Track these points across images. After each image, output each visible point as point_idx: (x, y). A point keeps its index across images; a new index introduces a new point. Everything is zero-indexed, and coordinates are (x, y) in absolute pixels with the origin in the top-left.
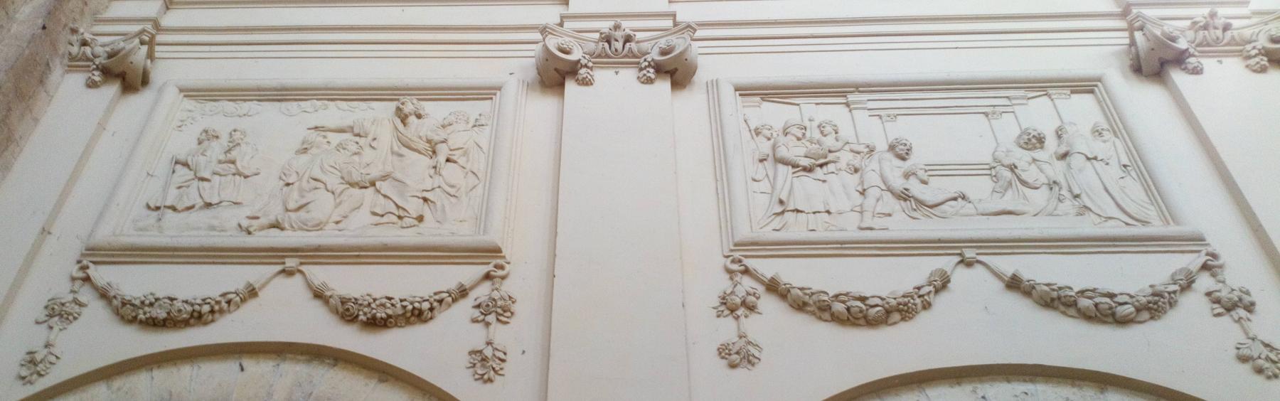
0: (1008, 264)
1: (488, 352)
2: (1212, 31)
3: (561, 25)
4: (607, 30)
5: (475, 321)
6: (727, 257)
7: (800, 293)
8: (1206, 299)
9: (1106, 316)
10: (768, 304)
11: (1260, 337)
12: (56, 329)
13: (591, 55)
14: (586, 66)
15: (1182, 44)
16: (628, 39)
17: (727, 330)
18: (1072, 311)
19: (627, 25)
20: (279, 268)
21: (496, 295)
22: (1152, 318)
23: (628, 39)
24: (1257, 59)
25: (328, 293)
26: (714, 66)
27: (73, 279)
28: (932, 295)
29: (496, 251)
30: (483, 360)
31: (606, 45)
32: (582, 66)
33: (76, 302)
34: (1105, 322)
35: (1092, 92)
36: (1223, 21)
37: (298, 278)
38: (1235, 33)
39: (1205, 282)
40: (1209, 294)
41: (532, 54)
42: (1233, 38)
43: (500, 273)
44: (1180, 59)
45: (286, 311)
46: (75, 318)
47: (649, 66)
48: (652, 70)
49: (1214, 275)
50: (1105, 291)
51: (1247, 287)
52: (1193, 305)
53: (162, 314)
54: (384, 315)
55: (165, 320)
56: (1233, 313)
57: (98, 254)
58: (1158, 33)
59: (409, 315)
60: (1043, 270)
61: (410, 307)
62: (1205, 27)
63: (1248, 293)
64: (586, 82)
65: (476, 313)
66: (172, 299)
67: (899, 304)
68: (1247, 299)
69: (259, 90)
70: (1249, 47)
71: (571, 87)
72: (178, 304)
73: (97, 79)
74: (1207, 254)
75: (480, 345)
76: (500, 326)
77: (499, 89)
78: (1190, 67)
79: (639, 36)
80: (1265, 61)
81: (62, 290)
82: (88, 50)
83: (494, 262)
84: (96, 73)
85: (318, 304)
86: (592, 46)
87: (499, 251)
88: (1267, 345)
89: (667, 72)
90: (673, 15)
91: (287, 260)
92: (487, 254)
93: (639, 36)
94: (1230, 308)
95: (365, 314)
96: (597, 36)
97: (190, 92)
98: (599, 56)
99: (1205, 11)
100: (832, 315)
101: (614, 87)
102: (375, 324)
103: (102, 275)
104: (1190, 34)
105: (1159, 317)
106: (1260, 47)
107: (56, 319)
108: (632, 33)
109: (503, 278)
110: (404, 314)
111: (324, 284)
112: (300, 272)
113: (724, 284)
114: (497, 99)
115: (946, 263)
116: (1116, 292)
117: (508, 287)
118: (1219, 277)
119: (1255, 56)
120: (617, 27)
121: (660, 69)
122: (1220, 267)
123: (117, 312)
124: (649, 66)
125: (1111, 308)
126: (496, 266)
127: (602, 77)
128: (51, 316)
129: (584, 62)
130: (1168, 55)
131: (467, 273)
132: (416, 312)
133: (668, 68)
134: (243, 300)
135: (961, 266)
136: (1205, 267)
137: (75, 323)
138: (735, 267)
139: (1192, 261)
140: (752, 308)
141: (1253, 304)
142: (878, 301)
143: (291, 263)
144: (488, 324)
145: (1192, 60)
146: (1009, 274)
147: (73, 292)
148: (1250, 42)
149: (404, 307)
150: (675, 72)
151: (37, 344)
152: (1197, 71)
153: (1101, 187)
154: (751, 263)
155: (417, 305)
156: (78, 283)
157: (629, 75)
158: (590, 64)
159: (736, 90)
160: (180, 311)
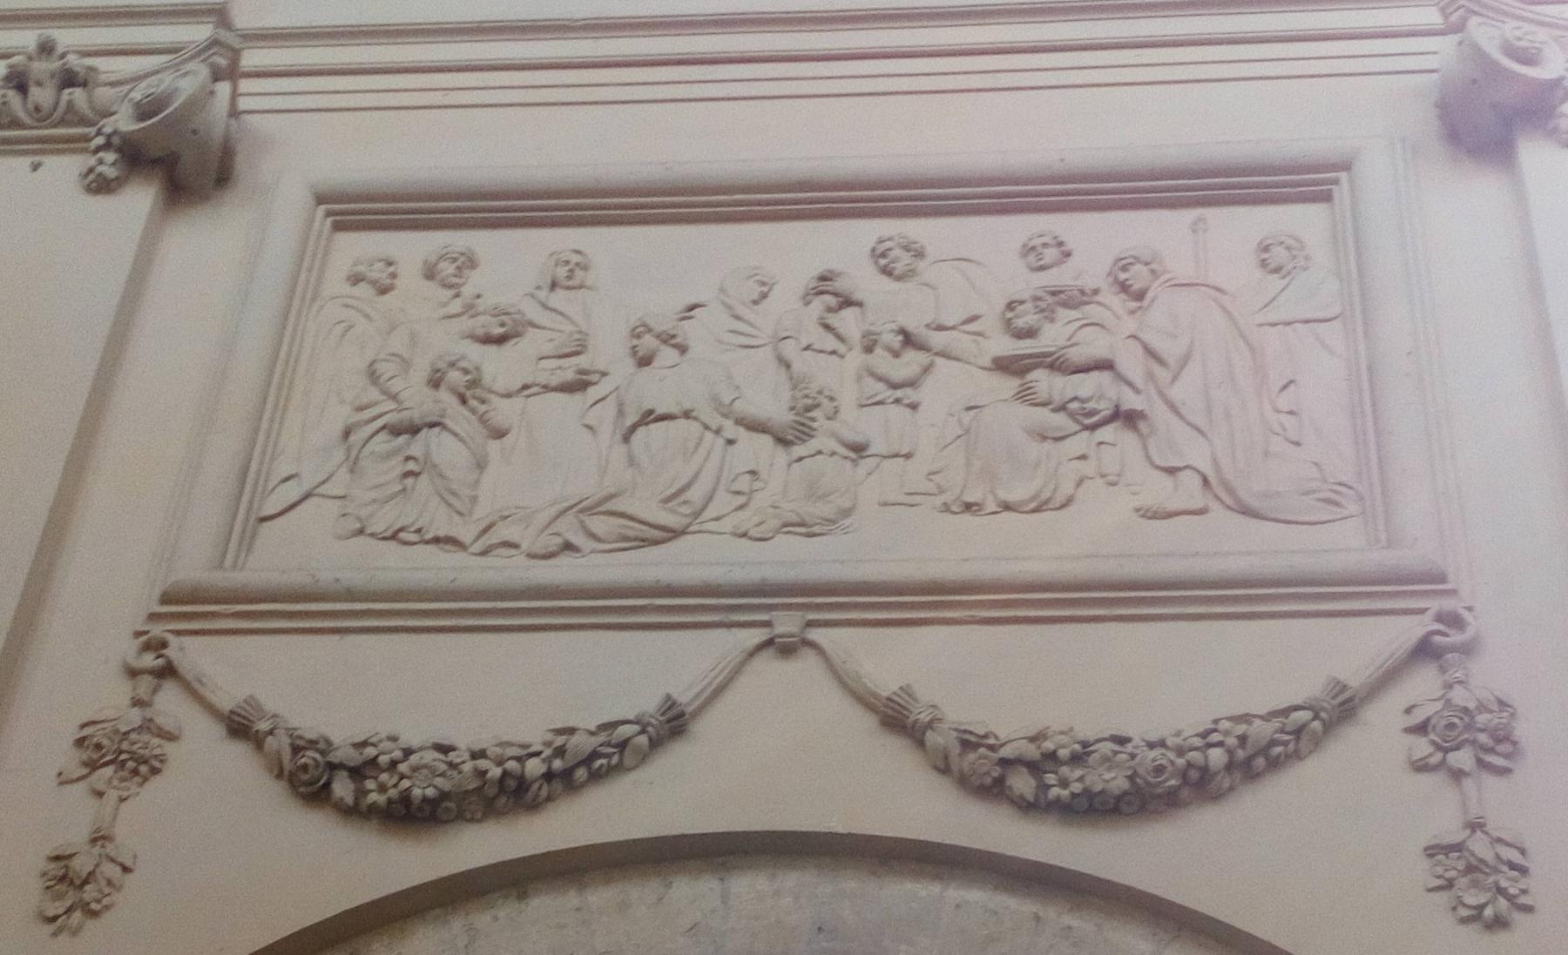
1: (1480, 847)
5: (1421, 767)
12: (113, 795)
16: (69, 79)
20: (756, 636)
21: (1459, 696)
26: (304, 143)
27: (133, 673)
29: (1433, 579)
30: (1470, 869)
33: (147, 726)
35: (1326, 197)
37: (807, 663)
45: (781, 747)
46: (155, 771)
47: (107, 146)
49: (1443, 670)
53: (1115, 781)
54: (430, 792)
55: (1119, 799)
59: (491, 791)
61: (496, 772)
73: (111, 172)
74: (1439, 618)
75: (1452, 831)
76: (1490, 780)
81: (111, 699)
82: (77, 95)
83: (1434, 605)
84: (110, 157)
87: (1442, 579)
89: (156, 162)
93: (110, 67)
95: (382, 789)
97: (354, 210)
102: (1095, 809)
107: (108, 771)
108: (73, 61)
110: (478, 790)
111: (251, 701)
112: (812, 645)
117: (1487, 677)
120: (46, 49)
124: (107, 146)
126: (1439, 618)
128: (93, 766)
131: (1356, 647)
132: (512, 784)
133: (155, 152)
134: (656, 744)
135: (768, 653)
137: (156, 783)
138: (149, 660)
143: (786, 624)
144: (1458, 775)
147: (137, 703)
149: (482, 774)
151: (75, 836)
155: (511, 765)
156: (146, 682)
159: (321, 199)
160: (1159, 770)
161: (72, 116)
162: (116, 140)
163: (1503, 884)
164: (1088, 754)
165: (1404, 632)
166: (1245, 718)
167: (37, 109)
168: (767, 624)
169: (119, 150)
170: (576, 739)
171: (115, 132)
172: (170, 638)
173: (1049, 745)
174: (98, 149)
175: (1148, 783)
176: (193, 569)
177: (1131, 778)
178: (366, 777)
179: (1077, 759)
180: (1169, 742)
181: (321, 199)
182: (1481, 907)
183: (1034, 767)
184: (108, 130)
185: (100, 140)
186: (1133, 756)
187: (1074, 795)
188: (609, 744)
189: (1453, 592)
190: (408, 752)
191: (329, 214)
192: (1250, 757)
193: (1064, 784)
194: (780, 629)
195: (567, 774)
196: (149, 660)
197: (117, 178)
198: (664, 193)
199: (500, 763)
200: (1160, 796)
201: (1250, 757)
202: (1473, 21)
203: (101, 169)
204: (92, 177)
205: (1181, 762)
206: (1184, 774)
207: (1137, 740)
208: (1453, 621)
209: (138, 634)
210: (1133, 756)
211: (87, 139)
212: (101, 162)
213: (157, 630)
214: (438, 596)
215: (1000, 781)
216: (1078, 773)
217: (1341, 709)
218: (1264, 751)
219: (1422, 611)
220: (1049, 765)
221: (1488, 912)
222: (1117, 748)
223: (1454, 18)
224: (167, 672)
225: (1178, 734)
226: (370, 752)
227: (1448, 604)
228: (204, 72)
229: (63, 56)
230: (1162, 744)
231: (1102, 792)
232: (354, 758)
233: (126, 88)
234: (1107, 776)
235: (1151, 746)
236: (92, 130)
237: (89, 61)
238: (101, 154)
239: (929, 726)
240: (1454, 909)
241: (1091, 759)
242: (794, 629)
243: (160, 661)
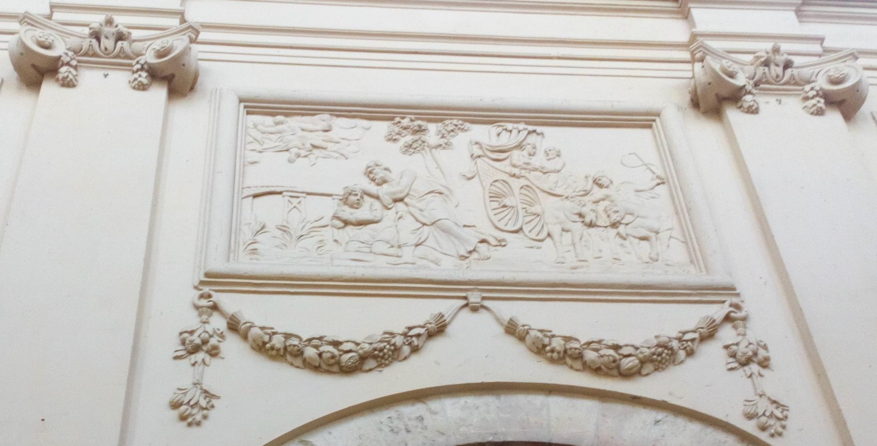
0: (508, 310)
2: (773, 67)
3: (50, 17)
4: (95, 25)
6: (196, 288)
7: (539, 335)
8: (724, 352)
9: (330, 365)
10: (232, 346)
11: (768, 394)
13: (76, 52)
14: (68, 64)
15: (740, 80)
16: (120, 37)
17: (183, 375)
18: (298, 362)
19: (121, 20)
20: (464, 302)
22: (656, 370)
23: (120, 37)
24: (814, 101)
26: (227, 75)
28: (696, 343)
29: (729, 289)
31: (94, 41)
32: (63, 65)
34: (613, 376)
35: (650, 127)
36: (786, 56)
37: (483, 315)
38: (795, 72)
39: (727, 334)
40: (726, 347)
41: (5, 46)
42: (792, 75)
44: (735, 97)
47: (142, 69)
48: (144, 74)
49: (735, 327)
50: (610, 343)
51: (765, 341)
52: (712, 354)
56: (746, 368)
57: (214, 280)
58: (717, 68)
60: (535, 315)
62: (766, 64)
63: (765, 347)
64: (68, 84)
67: (375, 349)
70: (807, 88)
71: (49, 88)
73: (145, 81)
74: (731, 305)
77: (658, 115)
78: (746, 105)
79: (136, 34)
80: (822, 103)
82: (125, 44)
83: (730, 300)
85: (511, 342)
86: (74, 42)
88: (774, 402)
90: (181, 15)
91: (469, 294)
94: (745, 363)
96: (86, 31)
97: (254, 106)
98: (86, 54)
99: (768, 45)
100: (304, 361)
101: (105, 94)
103: (230, 302)
104: (750, 70)
105: (663, 369)
106: (818, 88)
108: (125, 30)
113: (192, 320)
115: (446, 307)
116: (621, 344)
117: (755, 332)
118: (741, 330)
119: (813, 98)
120: (776, 51)
121: (155, 75)
122: (744, 319)
124: (142, 69)
125: (333, 357)
127: (767, 103)
129: (66, 59)
130: (724, 93)
135: (466, 310)
136: (727, 318)
138: (204, 302)
139: (717, 312)
140: (214, 352)
141: (767, 359)
142: (630, 350)
145: (748, 98)
146: (507, 318)
148: (809, 82)
150: (174, 79)
152: (753, 110)
153: (489, 224)
154: (217, 297)
157: (120, 79)
158: (74, 63)
159: (241, 101)
161: (122, 54)
162: (146, 67)
165: (725, 309)
167: (106, 49)
168: (465, 298)
169: (147, 71)
171: (146, 63)
172: (212, 293)
174: (138, 70)
176: (219, 265)
181: (241, 101)
184: (142, 62)
185: (139, 66)
189: (738, 295)
191: (245, 107)
198: (565, 113)
202: (708, 58)
203: (140, 79)
204: (136, 82)
208: (738, 307)
211: (131, 65)
212: (140, 76)
214: (331, 280)
219: (724, 302)
223: (698, 55)
224: (215, 307)
227: (735, 300)
228: (186, 39)
229: (117, 26)
233: (148, 43)
236: (134, 62)
237: (131, 31)
238: (139, 73)
242: (479, 300)
243: (211, 303)
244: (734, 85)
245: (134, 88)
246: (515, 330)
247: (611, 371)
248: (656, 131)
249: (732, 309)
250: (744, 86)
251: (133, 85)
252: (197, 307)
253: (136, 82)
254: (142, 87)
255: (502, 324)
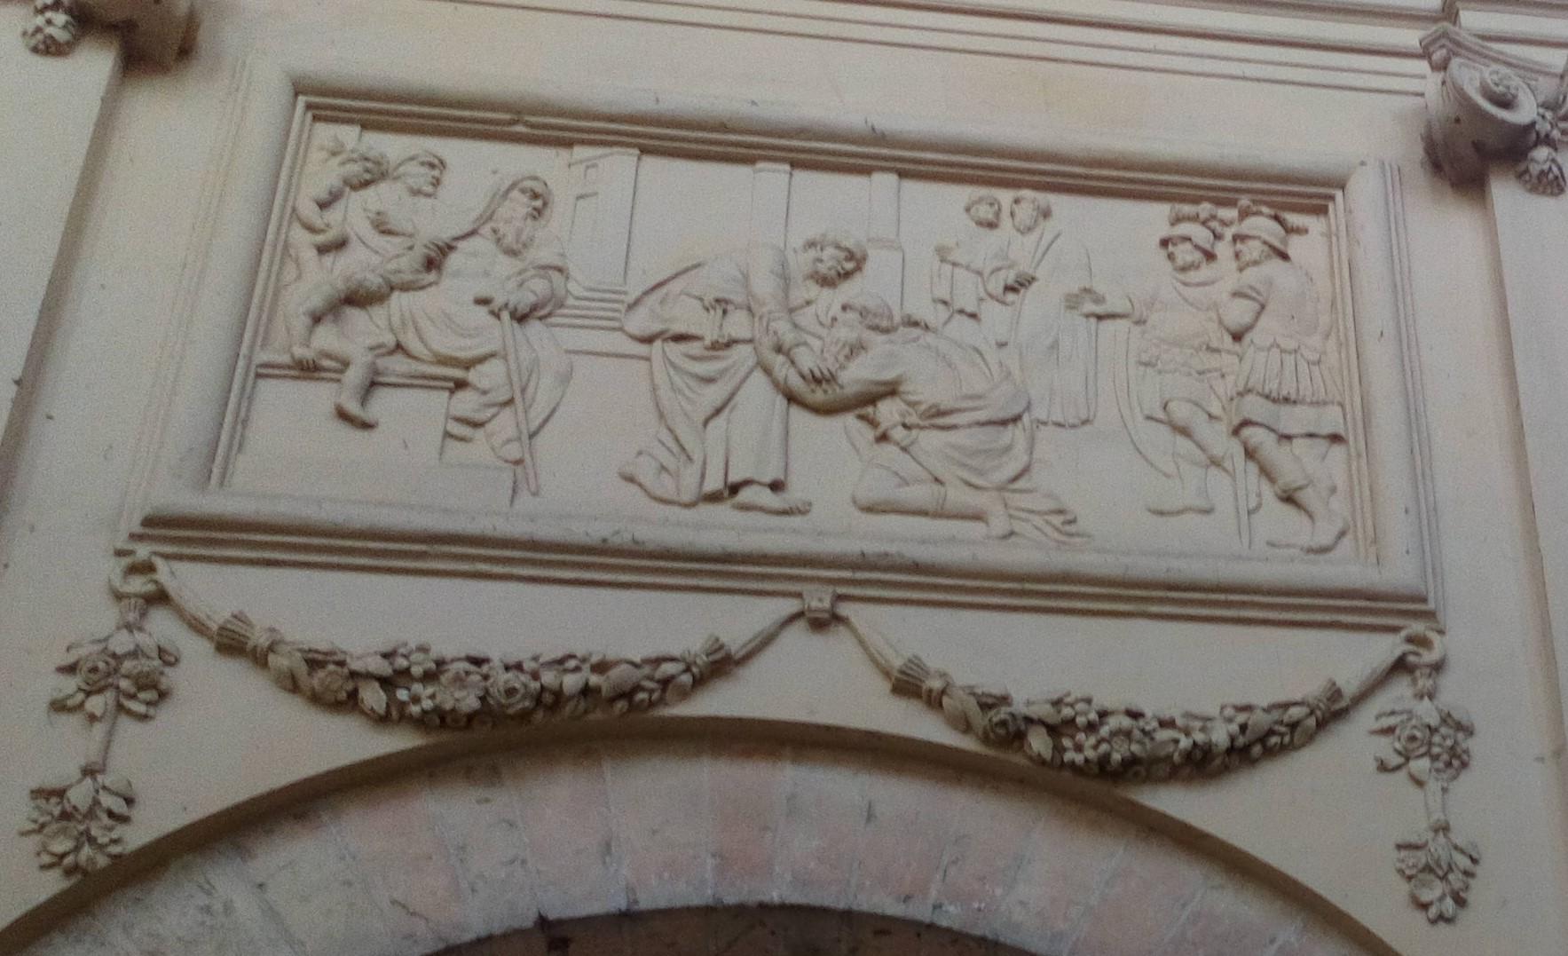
6: (120, 553)
25: (936, 684)
37: (837, 644)
43: (1429, 657)
48: (60, 18)
49: (1414, 681)
55: (471, 717)
65: (70, 686)
66: (477, 662)
68: (1465, 757)
69: (1387, 204)
72: (503, 679)
73: (61, 36)
75: (1418, 830)
78: (1535, 169)
81: (94, 621)
83: (1417, 627)
92: (1400, 610)
97: (327, 101)
109: (1438, 667)
111: (915, 662)
114: (1337, 207)
117: (1454, 693)
122: (1438, 667)
123: (292, 684)
129: (1544, 127)
131: (1351, 657)
134: (1321, 725)
135: (800, 627)
138: (138, 584)
145: (1542, 153)
159: (299, 88)
160: (510, 692)
163: (94, 832)
164: (442, 672)
165: (1385, 648)
166: (1247, 708)
169: (69, 11)
170: (614, 673)
173: (401, 663)
175: (499, 703)
177: (483, 699)
178: (397, 687)
179: (429, 677)
180: (526, 666)
181: (299, 88)
182: (63, 856)
183: (387, 683)
186: (486, 677)
187: (424, 712)
188: (650, 678)
190: (440, 663)
191: (309, 107)
192: (1256, 745)
193: (416, 700)
194: (815, 604)
195: (1246, 748)
196: (138, 584)
197: (68, 43)
199: (1187, 734)
200: (512, 717)
201: (1256, 745)
204: (40, 37)
205: (535, 685)
206: (538, 699)
207: (496, 662)
209: (120, 553)
210: (486, 677)
212: (49, 22)
213: (143, 551)
215: (353, 695)
216: (430, 690)
217: (1332, 711)
218: (1262, 739)
220: (401, 681)
221: (68, 860)
222: (472, 668)
224: (160, 598)
225: (535, 659)
226: (1067, 712)
230: (519, 667)
231: (453, 710)
232: (384, 668)
234: (458, 694)
235: (507, 668)
238: (49, 14)
239: (271, 648)
240: (38, 854)
241: (443, 679)
243: (151, 587)
244: (1503, 122)
245: (35, 50)
246: (920, 687)
247: (1098, 776)
248: (1332, 221)
249: (1410, 647)
250: (1533, 124)
251: (33, 42)
252: (119, 597)
253: (40, 37)
254: (50, 48)
255: (887, 674)
